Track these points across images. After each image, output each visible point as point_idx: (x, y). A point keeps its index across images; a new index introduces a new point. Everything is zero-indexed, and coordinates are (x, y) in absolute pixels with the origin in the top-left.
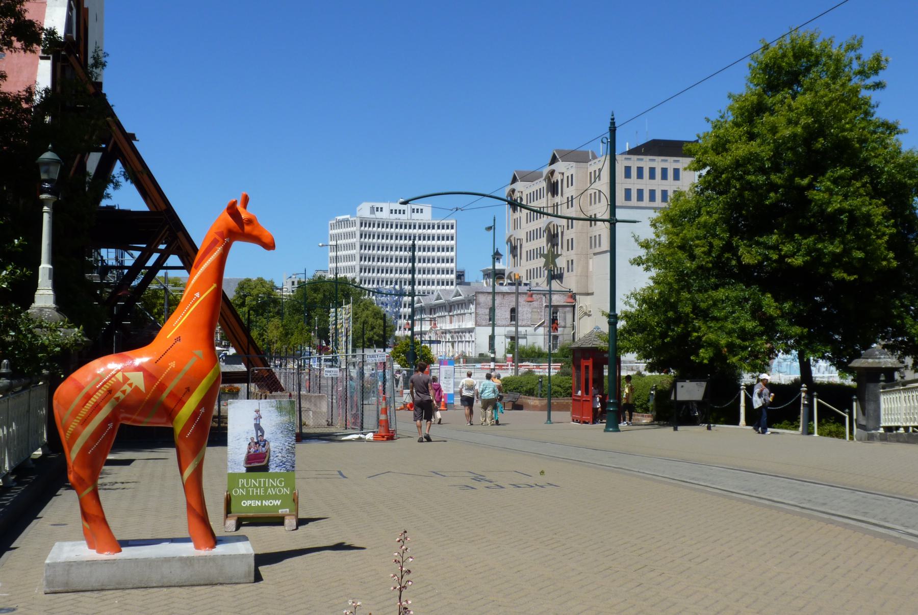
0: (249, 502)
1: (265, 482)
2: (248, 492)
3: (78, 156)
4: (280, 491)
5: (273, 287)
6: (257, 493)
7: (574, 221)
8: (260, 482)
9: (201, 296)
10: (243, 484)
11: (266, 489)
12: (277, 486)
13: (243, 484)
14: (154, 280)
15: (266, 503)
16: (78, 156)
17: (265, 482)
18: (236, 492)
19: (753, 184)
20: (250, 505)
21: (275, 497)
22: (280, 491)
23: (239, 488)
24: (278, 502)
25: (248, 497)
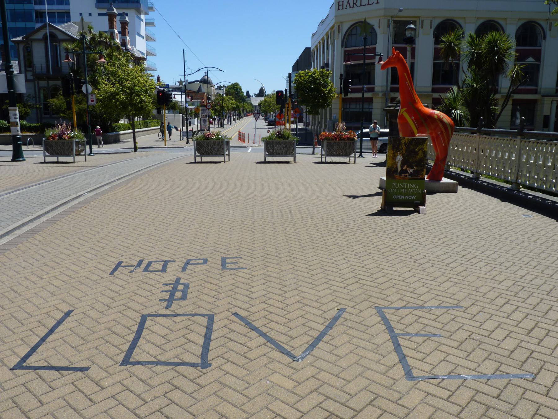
0: (397, 197)
1: (407, 185)
2: (397, 190)
3: (412, 209)
4: (416, 191)
5: (240, 89)
6: (402, 191)
7: (132, 134)
8: (404, 185)
9: (407, 81)
10: (394, 186)
11: (408, 190)
12: (414, 188)
13: (394, 186)
14: (139, 321)
15: (407, 197)
16: (412, 209)
17: (407, 185)
18: (390, 190)
19: (217, 114)
20: (398, 198)
21: (413, 194)
22: (416, 191)
23: (392, 188)
24: (414, 197)
25: (397, 194)
